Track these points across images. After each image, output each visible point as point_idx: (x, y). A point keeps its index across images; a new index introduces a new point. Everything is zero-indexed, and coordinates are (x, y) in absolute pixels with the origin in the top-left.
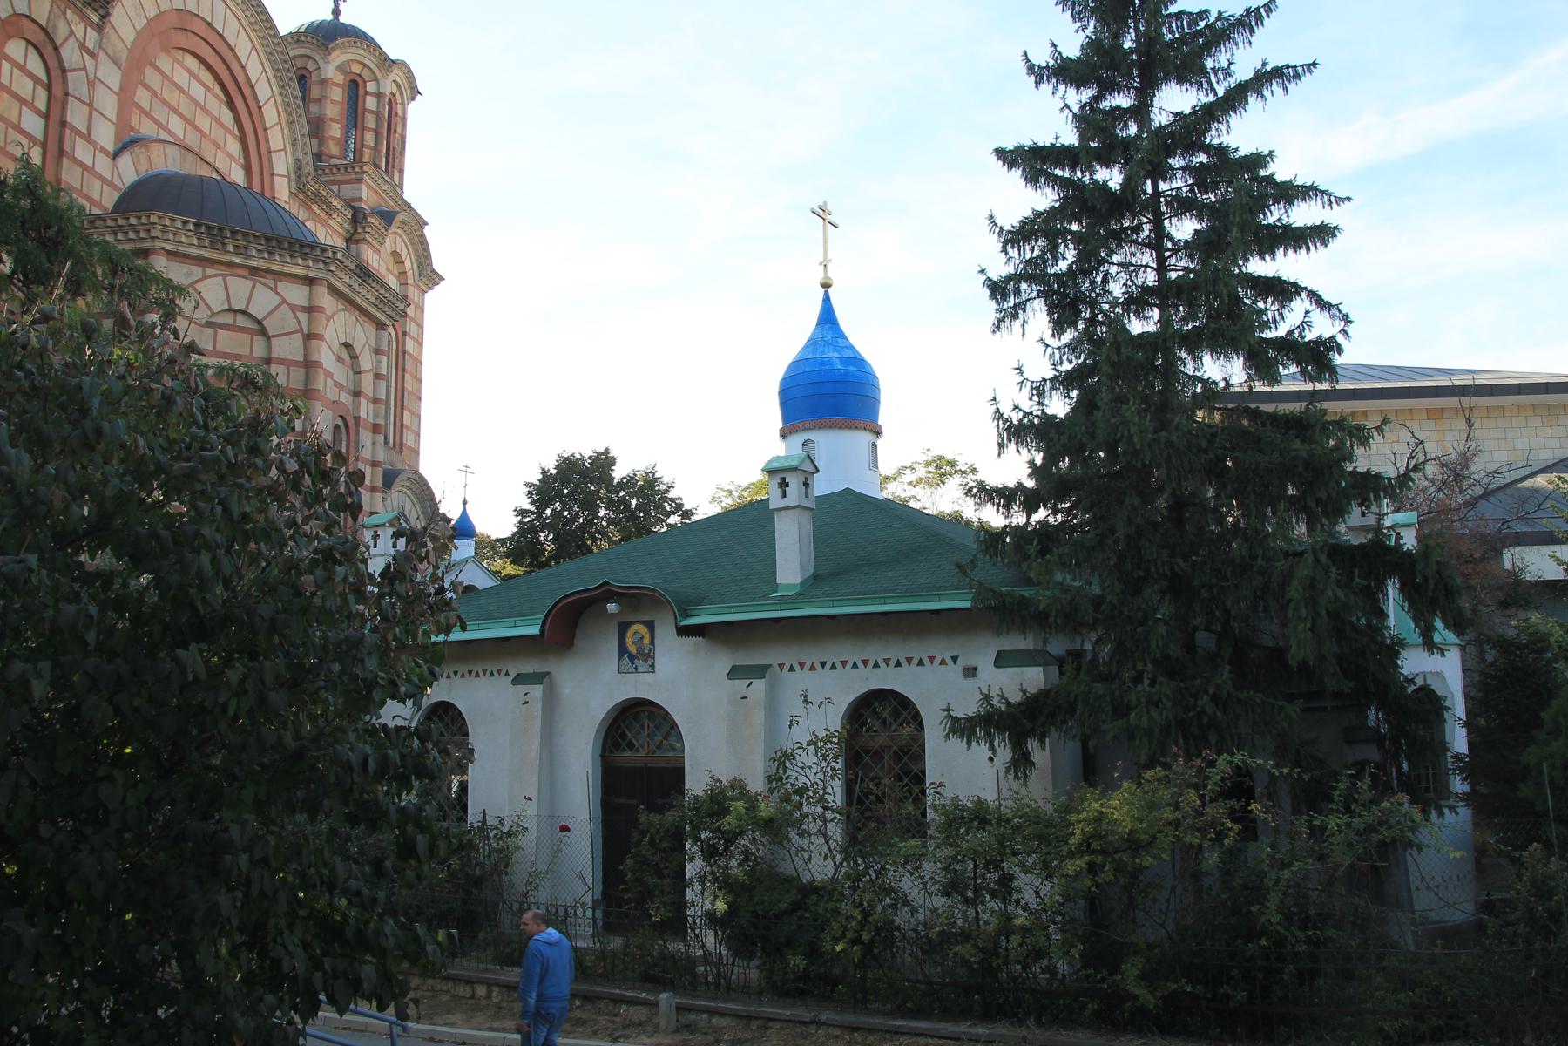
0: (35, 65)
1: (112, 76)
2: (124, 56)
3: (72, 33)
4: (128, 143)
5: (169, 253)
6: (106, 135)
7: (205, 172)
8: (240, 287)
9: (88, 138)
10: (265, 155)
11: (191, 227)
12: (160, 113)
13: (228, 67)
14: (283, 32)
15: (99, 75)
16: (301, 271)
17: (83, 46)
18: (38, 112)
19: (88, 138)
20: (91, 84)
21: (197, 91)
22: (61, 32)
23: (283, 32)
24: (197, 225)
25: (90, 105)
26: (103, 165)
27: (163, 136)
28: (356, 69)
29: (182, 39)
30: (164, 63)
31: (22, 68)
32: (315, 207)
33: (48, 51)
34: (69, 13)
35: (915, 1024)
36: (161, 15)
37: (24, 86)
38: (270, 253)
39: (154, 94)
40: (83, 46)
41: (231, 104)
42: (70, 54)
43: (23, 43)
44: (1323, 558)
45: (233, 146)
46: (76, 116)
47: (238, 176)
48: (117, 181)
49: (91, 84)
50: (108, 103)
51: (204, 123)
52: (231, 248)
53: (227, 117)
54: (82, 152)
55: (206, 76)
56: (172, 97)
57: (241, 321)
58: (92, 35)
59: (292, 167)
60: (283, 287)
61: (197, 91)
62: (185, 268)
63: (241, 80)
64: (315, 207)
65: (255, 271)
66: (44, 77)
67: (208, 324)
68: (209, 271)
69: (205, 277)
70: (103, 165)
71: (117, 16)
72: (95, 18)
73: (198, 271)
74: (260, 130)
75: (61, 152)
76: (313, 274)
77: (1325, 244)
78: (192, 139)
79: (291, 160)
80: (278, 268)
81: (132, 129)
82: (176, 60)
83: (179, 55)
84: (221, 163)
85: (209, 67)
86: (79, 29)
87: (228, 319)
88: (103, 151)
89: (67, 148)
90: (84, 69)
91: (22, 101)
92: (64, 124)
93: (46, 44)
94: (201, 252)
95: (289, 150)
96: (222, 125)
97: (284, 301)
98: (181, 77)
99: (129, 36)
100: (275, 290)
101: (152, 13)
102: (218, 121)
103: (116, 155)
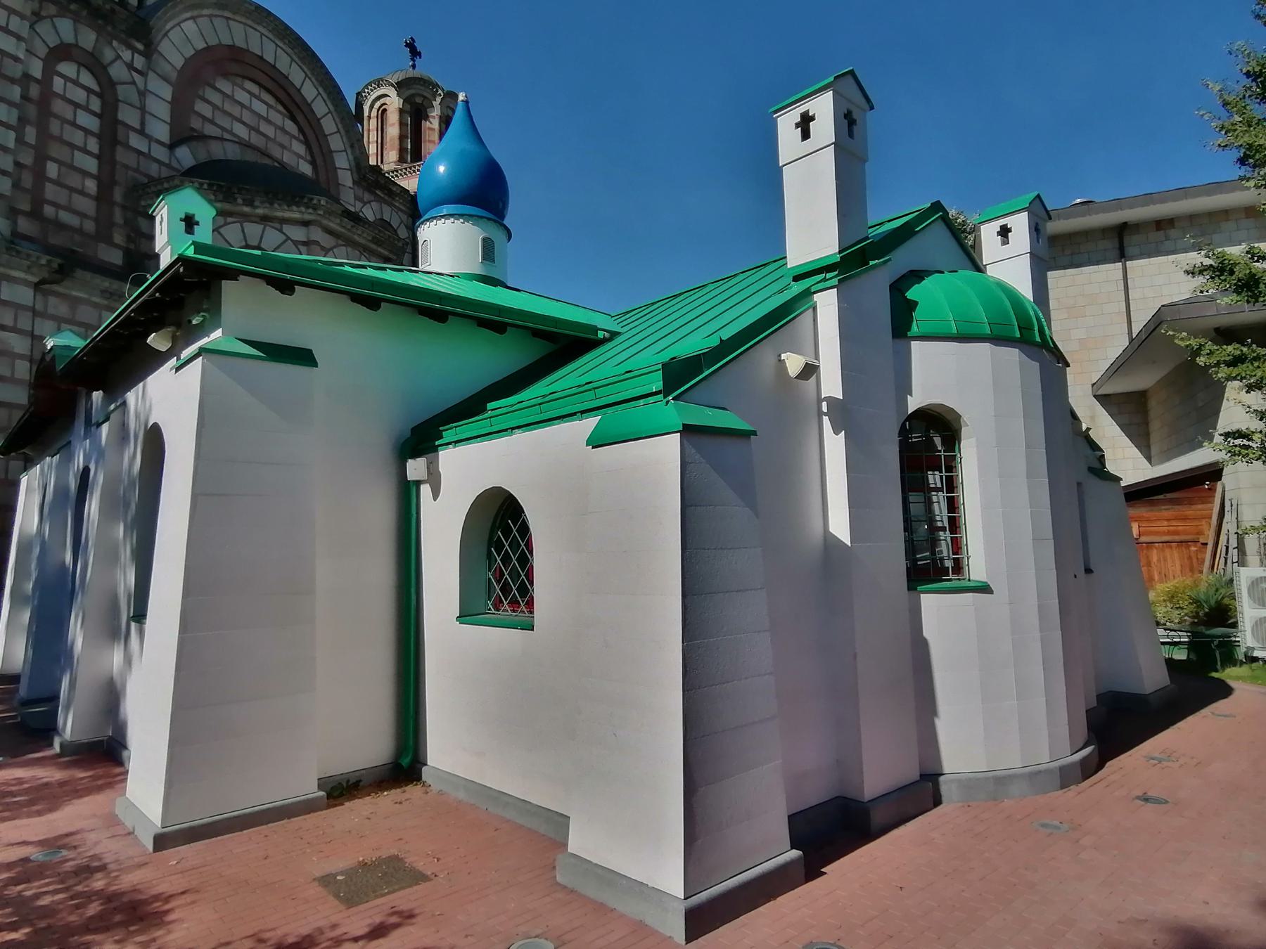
0: (87, 79)
1: (167, 92)
2: (174, 76)
3: (119, 57)
6: (161, 131)
7: (267, 161)
8: (253, 230)
9: (141, 132)
10: (328, 154)
11: (205, 186)
13: (285, 91)
14: (1050, 274)
15: (150, 87)
16: (296, 216)
17: (130, 66)
18: (56, 116)
19: (141, 132)
20: (143, 94)
22: (108, 55)
23: (1050, 274)
24: (209, 185)
26: (160, 153)
27: (227, 136)
28: (419, 100)
32: (378, 192)
34: (115, 43)
35: (413, 621)
36: (208, 49)
37: (79, 95)
38: (272, 204)
39: (215, 107)
40: (130, 66)
41: (293, 119)
45: (299, 148)
46: (128, 115)
47: (306, 169)
48: (175, 164)
50: (161, 108)
51: (264, 128)
52: (240, 201)
53: (290, 126)
54: (135, 141)
55: (280, 108)
56: (236, 111)
58: (139, 62)
59: (353, 163)
60: (286, 228)
63: (298, 99)
64: (378, 192)
65: (265, 219)
66: (96, 88)
68: (230, 220)
69: (226, 224)
70: (160, 153)
71: (165, 47)
72: (140, 46)
74: (321, 137)
76: (307, 217)
78: (256, 140)
79: (351, 157)
80: (279, 214)
81: (193, 129)
82: (234, 84)
83: (239, 80)
84: (287, 158)
86: (126, 55)
89: (120, 136)
90: (134, 83)
92: (116, 122)
95: (349, 151)
96: (286, 132)
97: (288, 238)
98: (242, 96)
99: (179, 62)
100: (281, 231)
101: (201, 45)
102: (282, 129)
103: (172, 146)
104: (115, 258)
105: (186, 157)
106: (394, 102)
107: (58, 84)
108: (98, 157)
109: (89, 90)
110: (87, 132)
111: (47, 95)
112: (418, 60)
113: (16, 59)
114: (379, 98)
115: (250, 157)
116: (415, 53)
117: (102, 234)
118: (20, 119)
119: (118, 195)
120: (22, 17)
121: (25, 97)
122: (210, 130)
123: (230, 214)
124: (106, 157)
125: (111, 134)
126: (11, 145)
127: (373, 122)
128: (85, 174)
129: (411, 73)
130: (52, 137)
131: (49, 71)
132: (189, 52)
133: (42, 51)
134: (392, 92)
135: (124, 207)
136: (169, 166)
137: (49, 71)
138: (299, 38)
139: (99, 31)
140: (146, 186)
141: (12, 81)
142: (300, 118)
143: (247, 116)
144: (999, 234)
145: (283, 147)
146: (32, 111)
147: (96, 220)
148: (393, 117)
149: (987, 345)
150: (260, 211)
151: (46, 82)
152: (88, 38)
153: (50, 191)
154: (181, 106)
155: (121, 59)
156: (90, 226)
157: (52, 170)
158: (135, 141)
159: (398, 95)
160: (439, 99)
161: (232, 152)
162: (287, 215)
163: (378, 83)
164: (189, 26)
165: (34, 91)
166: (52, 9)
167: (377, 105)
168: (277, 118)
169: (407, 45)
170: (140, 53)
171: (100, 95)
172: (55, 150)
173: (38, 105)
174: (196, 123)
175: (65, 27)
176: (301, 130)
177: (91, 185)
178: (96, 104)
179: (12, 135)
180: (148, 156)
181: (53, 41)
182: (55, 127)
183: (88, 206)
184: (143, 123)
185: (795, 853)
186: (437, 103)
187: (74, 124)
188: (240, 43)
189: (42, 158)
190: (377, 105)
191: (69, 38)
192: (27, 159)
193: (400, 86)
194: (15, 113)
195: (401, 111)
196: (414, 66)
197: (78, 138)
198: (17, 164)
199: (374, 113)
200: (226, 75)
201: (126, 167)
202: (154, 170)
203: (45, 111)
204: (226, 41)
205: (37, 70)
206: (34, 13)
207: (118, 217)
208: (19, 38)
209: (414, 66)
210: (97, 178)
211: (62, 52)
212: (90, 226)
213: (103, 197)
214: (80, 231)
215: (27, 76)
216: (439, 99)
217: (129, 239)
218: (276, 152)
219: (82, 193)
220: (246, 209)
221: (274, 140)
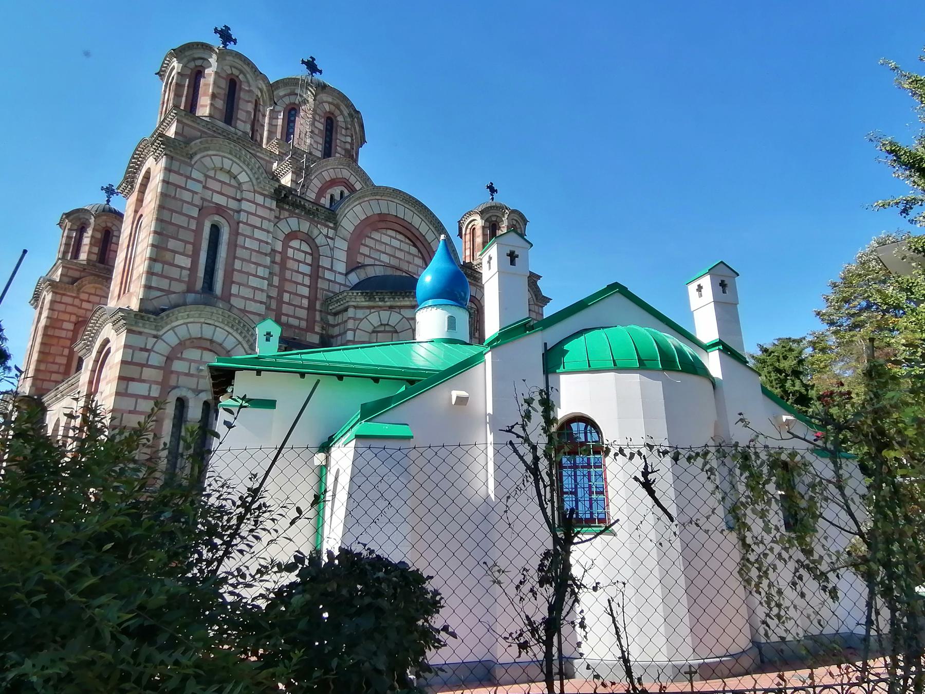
1: (344, 245)
4: (353, 267)
5: (355, 307)
6: (341, 267)
7: (398, 273)
8: (385, 315)
12: (375, 255)
16: (408, 303)
17: (327, 236)
18: (289, 269)
19: (331, 270)
20: (332, 249)
21: (396, 243)
24: (362, 293)
25: (332, 258)
26: (340, 279)
27: (377, 263)
28: (494, 219)
29: (383, 225)
30: (376, 235)
31: (299, 250)
33: (310, 241)
37: (301, 256)
39: (371, 248)
40: (327, 236)
41: (415, 245)
42: (320, 240)
43: (299, 241)
44: (199, 63)
46: (325, 262)
48: (348, 283)
49: (332, 249)
50: (342, 256)
51: (399, 254)
53: (413, 250)
55: (407, 241)
56: (382, 248)
57: (387, 328)
58: (331, 233)
61: (396, 243)
62: (362, 311)
65: (391, 308)
67: (373, 332)
70: (340, 279)
72: (331, 225)
73: (368, 311)
75: (318, 277)
77: (433, 605)
78: (394, 262)
80: (398, 304)
83: (384, 231)
85: (400, 233)
86: (325, 231)
87: (382, 329)
88: (339, 273)
89: (320, 274)
91: (299, 262)
92: (319, 266)
93: (308, 239)
94: (366, 304)
98: (385, 239)
99: (351, 228)
102: (409, 253)
103: (346, 274)
104: (316, 339)
105: (354, 278)
106: (479, 222)
107: (290, 252)
108: (309, 287)
109: (306, 253)
110: (304, 274)
111: (285, 258)
112: (495, 195)
113: (267, 243)
114: (471, 222)
115: (389, 272)
116: (492, 190)
117: (310, 329)
118: (270, 273)
119: (318, 306)
120: (269, 221)
121: (273, 262)
122: (368, 261)
123: (373, 307)
124: (313, 287)
125: (316, 272)
126: (265, 288)
127: (468, 237)
128: (303, 296)
129: (490, 203)
130: (287, 280)
131: (286, 246)
132: (357, 222)
133: (282, 237)
134: (478, 217)
135: (321, 311)
136: (345, 285)
137: (286, 246)
138: (417, 201)
139: (312, 221)
140: (332, 298)
141: (266, 255)
142: (419, 244)
143: (388, 250)
144: (720, 285)
145: (409, 263)
146: (277, 269)
147: (307, 320)
148: (479, 232)
149: (613, 374)
150: (388, 304)
151: (284, 253)
152: (305, 226)
153: (285, 309)
154: (352, 251)
155: (321, 233)
156: (304, 324)
157: (286, 297)
158: (328, 275)
159: (482, 218)
160: (506, 216)
161: (379, 271)
162: (403, 303)
163: (470, 213)
164: (358, 209)
165: (278, 258)
166: (286, 214)
167: (470, 226)
168: (405, 247)
169: (488, 187)
170: (331, 228)
171: (311, 254)
172: (288, 287)
173: (281, 263)
174: (360, 259)
175: (293, 222)
176: (419, 251)
177: (305, 302)
178: (309, 259)
179: (266, 282)
180: (334, 282)
181: (287, 231)
182: (288, 274)
183: (303, 313)
184: (332, 266)
185: (220, 591)
186: (505, 219)
187: (298, 272)
188: (385, 211)
189: (281, 291)
190: (470, 226)
191: (295, 227)
192: (274, 293)
193: (482, 213)
194: (267, 271)
195: (483, 228)
196: (493, 199)
197: (299, 278)
198: (269, 297)
199: (468, 231)
200: (377, 230)
201: (323, 289)
202: (336, 288)
203: (283, 266)
204: (377, 211)
205: (279, 247)
206: (276, 217)
207: (318, 318)
208: (268, 232)
209: (493, 199)
210: (308, 298)
211: (292, 235)
212: (304, 324)
213: (311, 308)
214: (298, 328)
215: (273, 250)
216: (506, 216)
217: (323, 328)
218: (405, 266)
219: (301, 307)
220: (381, 304)
221: (404, 260)
